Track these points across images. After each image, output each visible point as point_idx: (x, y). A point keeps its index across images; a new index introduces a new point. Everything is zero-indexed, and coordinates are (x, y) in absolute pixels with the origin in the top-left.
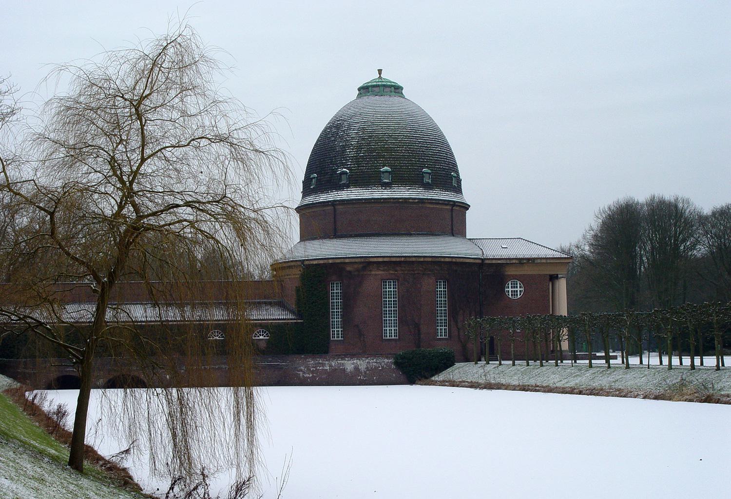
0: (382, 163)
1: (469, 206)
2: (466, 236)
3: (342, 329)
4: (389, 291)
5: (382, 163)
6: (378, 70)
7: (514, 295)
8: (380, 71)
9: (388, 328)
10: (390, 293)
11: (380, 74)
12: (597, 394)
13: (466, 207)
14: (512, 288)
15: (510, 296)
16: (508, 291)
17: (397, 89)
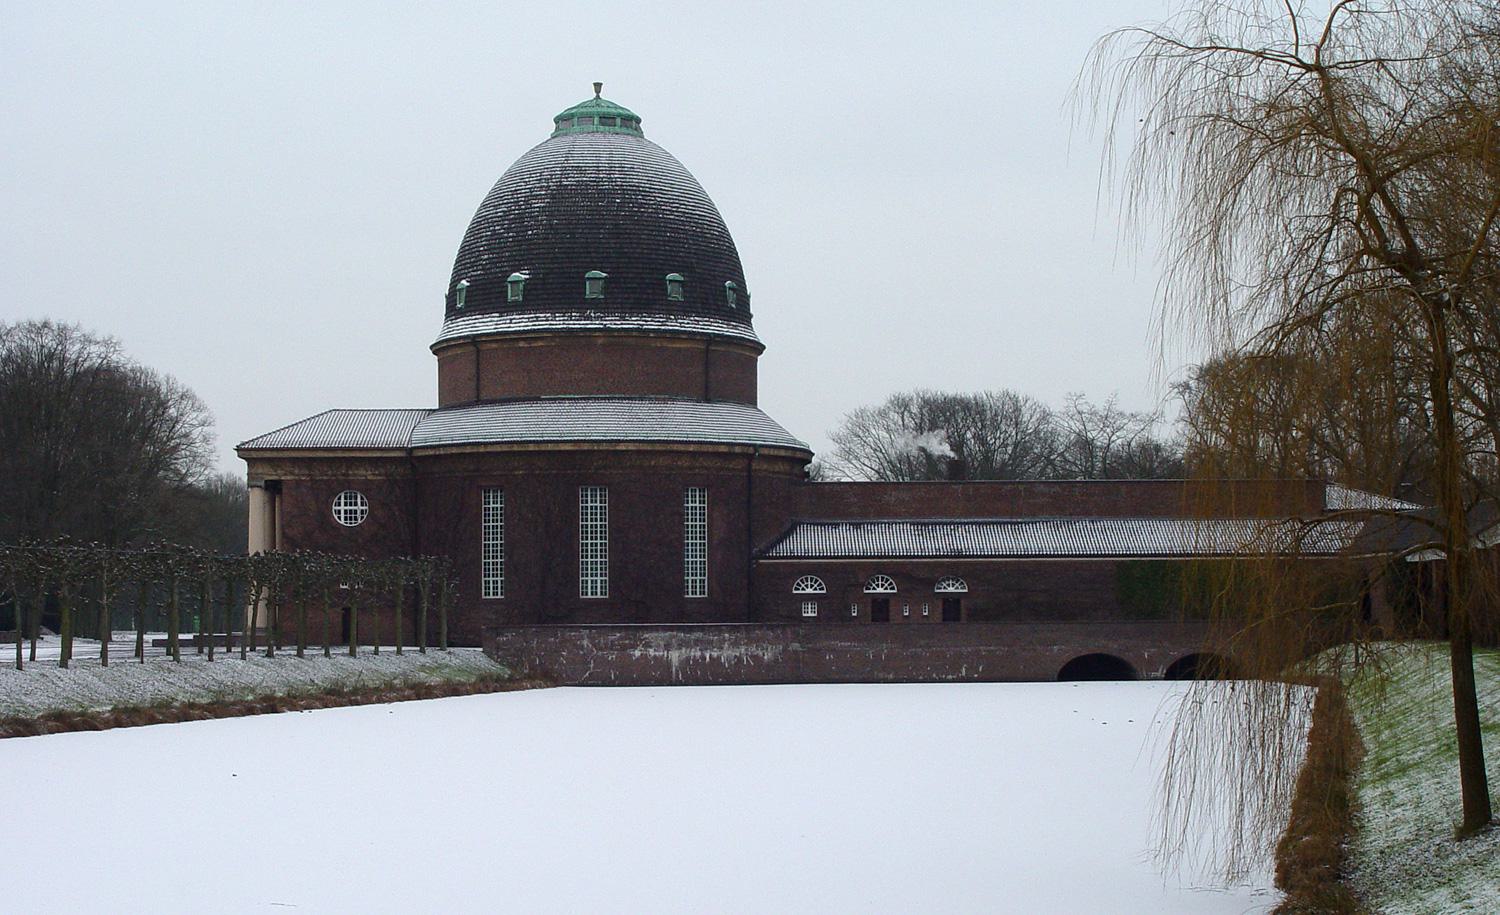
0: (602, 260)
1: (764, 347)
2: (756, 404)
3: (686, 578)
4: (592, 507)
5: (602, 260)
6: (595, 84)
7: (351, 519)
8: (598, 86)
9: (589, 578)
10: (594, 511)
11: (598, 91)
12: (152, 721)
13: (759, 348)
14: (346, 505)
15: (342, 522)
16: (339, 512)
17: (630, 122)
